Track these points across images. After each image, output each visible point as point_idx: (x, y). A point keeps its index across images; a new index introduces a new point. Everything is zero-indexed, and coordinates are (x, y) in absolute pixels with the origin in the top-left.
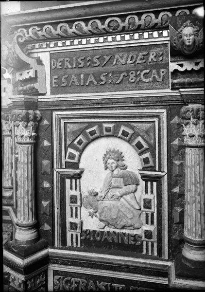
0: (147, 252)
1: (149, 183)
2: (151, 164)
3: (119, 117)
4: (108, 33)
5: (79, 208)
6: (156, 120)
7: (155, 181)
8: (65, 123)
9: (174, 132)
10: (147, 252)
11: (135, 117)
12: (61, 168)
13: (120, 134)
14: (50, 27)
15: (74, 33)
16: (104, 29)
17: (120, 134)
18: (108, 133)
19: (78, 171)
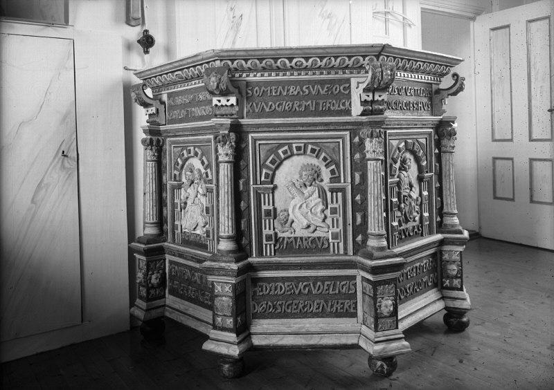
0: (334, 251)
1: (335, 194)
3: (404, 135)
4: (311, 69)
5: (272, 221)
6: (341, 141)
8: (259, 144)
9: (358, 147)
10: (334, 251)
12: (256, 184)
13: (295, 152)
14: (272, 61)
16: (291, 66)
17: (295, 152)
18: (286, 155)
19: (272, 186)
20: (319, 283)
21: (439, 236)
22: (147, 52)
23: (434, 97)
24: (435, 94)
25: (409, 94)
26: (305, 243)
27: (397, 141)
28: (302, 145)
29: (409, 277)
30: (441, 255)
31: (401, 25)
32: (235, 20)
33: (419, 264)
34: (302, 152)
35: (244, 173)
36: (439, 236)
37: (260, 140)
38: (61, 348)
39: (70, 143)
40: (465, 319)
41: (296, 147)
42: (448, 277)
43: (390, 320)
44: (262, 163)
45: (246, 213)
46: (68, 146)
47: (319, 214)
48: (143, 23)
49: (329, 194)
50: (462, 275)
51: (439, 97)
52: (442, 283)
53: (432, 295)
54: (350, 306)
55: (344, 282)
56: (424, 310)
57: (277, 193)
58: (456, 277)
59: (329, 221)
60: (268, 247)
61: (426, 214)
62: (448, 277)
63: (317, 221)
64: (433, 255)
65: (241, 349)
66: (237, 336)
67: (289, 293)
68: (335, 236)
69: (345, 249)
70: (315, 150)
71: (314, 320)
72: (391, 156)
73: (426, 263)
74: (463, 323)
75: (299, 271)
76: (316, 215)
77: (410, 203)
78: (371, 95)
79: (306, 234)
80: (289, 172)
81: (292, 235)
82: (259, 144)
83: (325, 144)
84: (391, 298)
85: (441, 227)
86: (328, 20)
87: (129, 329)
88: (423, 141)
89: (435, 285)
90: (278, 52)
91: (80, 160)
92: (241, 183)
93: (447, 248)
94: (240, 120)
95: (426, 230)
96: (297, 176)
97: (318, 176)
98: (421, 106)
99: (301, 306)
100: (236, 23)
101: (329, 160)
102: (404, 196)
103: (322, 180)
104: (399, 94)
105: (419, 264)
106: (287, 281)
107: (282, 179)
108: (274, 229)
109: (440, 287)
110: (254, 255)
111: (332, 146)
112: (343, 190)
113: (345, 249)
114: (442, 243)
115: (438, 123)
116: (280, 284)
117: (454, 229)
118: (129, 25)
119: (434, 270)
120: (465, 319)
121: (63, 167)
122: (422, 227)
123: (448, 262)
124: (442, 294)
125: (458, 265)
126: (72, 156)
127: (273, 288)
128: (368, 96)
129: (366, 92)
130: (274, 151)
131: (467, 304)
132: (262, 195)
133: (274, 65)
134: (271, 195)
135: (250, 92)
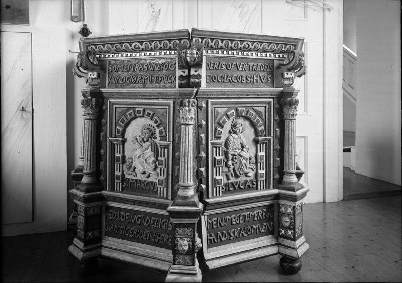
1: (163, 149)
2: (164, 134)
3: (233, 104)
7: (166, 148)
8: (116, 108)
11: (222, 104)
12: (112, 137)
15: (132, 49)
20: (148, 218)
21: (276, 191)
22: (302, 40)
23: (274, 72)
24: (277, 69)
25: (240, 69)
26: (142, 185)
27: (225, 109)
28: (142, 109)
29: (234, 223)
30: (279, 208)
31: (322, 10)
32: (154, 13)
33: (248, 213)
34: (141, 115)
35: (104, 128)
36: (276, 191)
37: (116, 104)
38: (18, 236)
39: (27, 101)
40: (297, 265)
41: (148, 113)
42: (283, 227)
43: (188, 258)
44: (117, 121)
45: (103, 158)
46: (26, 103)
47: (151, 164)
48: (84, 20)
49: (160, 149)
50: (294, 227)
51: (280, 71)
52: (280, 232)
53: (266, 240)
54: (168, 240)
55: (164, 220)
56: (251, 252)
57: (126, 145)
58: (289, 228)
59: (158, 170)
60: (118, 184)
61: (262, 172)
62: (283, 227)
63: (149, 170)
64: (269, 207)
65: (85, 255)
66: (85, 246)
67: (128, 221)
68: (161, 183)
69: (167, 194)
70: (150, 114)
71: (143, 245)
72: (217, 121)
73: (258, 213)
74: (294, 268)
75: (133, 206)
76: (149, 164)
77: (240, 161)
78: (186, 71)
79: (143, 178)
80: (135, 129)
81: (135, 178)
82: (116, 108)
83: (158, 110)
84: (188, 239)
85: (279, 183)
86: (240, 10)
87: (66, 230)
88: (262, 109)
89: (270, 232)
90: (119, 38)
91: (34, 114)
92: (177, 136)
93: (282, 202)
94: (101, 89)
95: (261, 184)
96: (139, 134)
97: (152, 134)
98: (258, 79)
99: (135, 233)
100: (155, 18)
101: (159, 122)
102: (233, 155)
103: (155, 138)
104: (227, 69)
105: (248, 213)
106: (128, 212)
107: (130, 135)
108: (123, 171)
109: (276, 234)
110: (108, 189)
111: (162, 111)
112: (167, 147)
113: (167, 194)
114: (277, 197)
115: (278, 93)
116: (123, 213)
117: (289, 186)
118: (74, 21)
119: (270, 219)
120: (297, 265)
121: (22, 117)
122: (257, 182)
123: (284, 214)
124: (278, 241)
125: (291, 218)
126: (28, 111)
127: (118, 216)
128: (184, 72)
129: (182, 69)
130: (124, 113)
131: (301, 252)
132: (116, 146)
133: (130, 48)
134: (121, 146)
135: (110, 68)
